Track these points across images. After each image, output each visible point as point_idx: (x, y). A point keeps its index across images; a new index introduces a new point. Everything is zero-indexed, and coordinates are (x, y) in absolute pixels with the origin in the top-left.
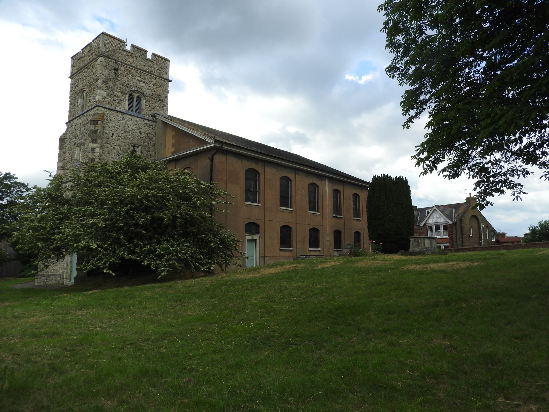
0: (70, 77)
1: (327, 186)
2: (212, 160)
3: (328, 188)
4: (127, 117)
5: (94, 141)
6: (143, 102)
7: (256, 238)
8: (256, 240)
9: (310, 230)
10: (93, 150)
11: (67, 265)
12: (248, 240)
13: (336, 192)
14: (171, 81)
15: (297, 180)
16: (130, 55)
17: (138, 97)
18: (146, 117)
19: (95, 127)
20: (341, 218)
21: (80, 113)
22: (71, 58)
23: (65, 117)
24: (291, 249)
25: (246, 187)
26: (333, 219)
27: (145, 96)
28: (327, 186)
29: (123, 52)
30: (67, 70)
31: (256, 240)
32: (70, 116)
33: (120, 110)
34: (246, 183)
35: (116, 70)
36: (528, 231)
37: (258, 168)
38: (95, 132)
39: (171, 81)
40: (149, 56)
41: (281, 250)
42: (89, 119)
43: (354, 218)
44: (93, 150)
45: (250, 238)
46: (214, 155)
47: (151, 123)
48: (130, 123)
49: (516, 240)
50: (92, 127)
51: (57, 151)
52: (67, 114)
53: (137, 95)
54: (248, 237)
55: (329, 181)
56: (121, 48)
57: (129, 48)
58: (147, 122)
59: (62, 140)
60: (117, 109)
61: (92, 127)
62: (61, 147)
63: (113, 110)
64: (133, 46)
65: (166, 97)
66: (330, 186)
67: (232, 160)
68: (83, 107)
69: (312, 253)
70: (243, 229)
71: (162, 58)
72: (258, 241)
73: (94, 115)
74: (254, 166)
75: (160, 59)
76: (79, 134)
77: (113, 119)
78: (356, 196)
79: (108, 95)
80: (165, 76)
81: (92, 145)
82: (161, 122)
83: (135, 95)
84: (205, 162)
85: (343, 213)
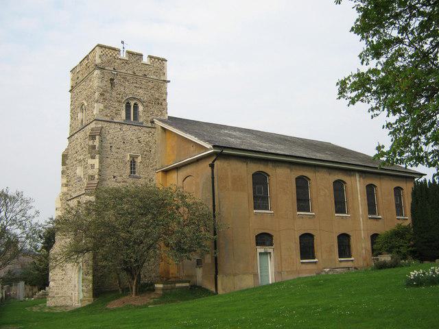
0: (70, 91)
1: (358, 182)
2: (212, 166)
3: (360, 184)
4: (125, 127)
5: (93, 158)
6: (141, 108)
7: (269, 250)
8: (270, 253)
9: (339, 237)
10: (93, 166)
11: (75, 286)
12: (260, 254)
13: (370, 190)
14: (169, 82)
15: (211, 207)
17: (135, 104)
18: (145, 124)
20: (380, 218)
21: (80, 126)
24: (315, 260)
25: (254, 193)
26: (369, 221)
28: (358, 182)
29: (118, 61)
31: (270, 253)
32: (71, 131)
33: (118, 121)
34: (254, 188)
35: (112, 80)
38: (94, 147)
39: (169, 82)
40: (145, 60)
41: (302, 263)
42: (88, 134)
43: (398, 217)
44: (93, 166)
45: (262, 251)
46: (214, 161)
48: (129, 133)
49: (77, 310)
50: (91, 143)
51: (60, 168)
52: (68, 129)
53: (134, 102)
54: (260, 250)
55: (360, 176)
56: (116, 57)
58: (146, 129)
59: (65, 157)
60: (115, 120)
61: (91, 143)
62: (64, 164)
63: (110, 122)
66: (362, 180)
68: (82, 121)
69: (343, 265)
70: (254, 241)
71: (159, 59)
72: (272, 254)
73: (92, 129)
75: (156, 60)
76: (79, 149)
78: (398, 190)
79: (105, 107)
81: (91, 161)
82: (160, 128)
83: (132, 103)
84: (205, 167)
85: (381, 213)
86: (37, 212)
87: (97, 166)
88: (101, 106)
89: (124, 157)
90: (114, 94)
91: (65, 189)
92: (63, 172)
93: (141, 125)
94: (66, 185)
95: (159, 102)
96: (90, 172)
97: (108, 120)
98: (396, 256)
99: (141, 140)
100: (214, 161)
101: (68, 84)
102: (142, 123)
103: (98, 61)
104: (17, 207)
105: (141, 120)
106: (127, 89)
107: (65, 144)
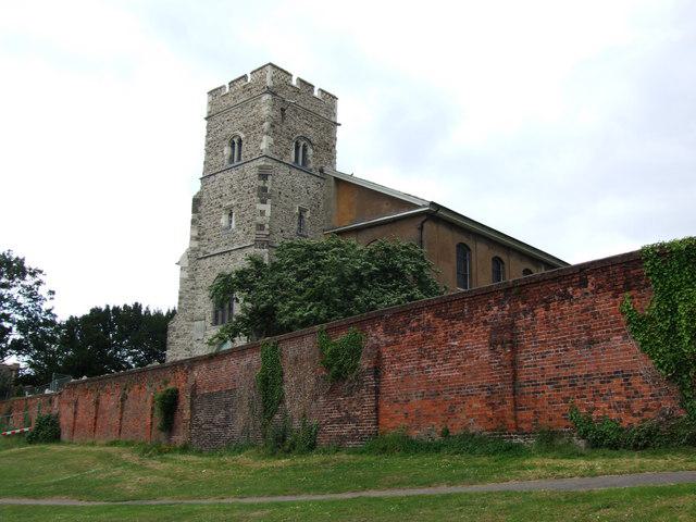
0: (206, 119)
2: (421, 229)
4: (294, 172)
5: (264, 202)
6: (310, 151)
10: (262, 213)
16: (297, 91)
19: (265, 182)
22: (210, 93)
23: (198, 170)
27: (312, 144)
30: (203, 109)
32: (206, 170)
36: (104, 308)
37: (470, 243)
38: (265, 189)
40: (316, 94)
44: (262, 213)
46: (423, 222)
47: (319, 180)
48: (297, 180)
50: (261, 183)
51: (189, 216)
57: (294, 83)
59: (197, 202)
61: (261, 183)
62: (195, 210)
64: (301, 81)
65: (334, 146)
67: (443, 230)
71: (330, 95)
74: (465, 240)
77: (280, 173)
79: (275, 142)
80: (333, 119)
81: (260, 207)
86: (52, 292)
87: (268, 213)
88: (271, 140)
89: (293, 208)
90: (284, 128)
91: (196, 244)
92: (193, 222)
93: (309, 172)
94: (197, 239)
95: (328, 148)
96: (259, 219)
97: (276, 157)
98: (243, 371)
99: (310, 190)
100: (423, 222)
101: (204, 111)
102: (311, 170)
103: (269, 83)
104: (29, 281)
105: (311, 166)
106: (298, 125)
107: (196, 187)
